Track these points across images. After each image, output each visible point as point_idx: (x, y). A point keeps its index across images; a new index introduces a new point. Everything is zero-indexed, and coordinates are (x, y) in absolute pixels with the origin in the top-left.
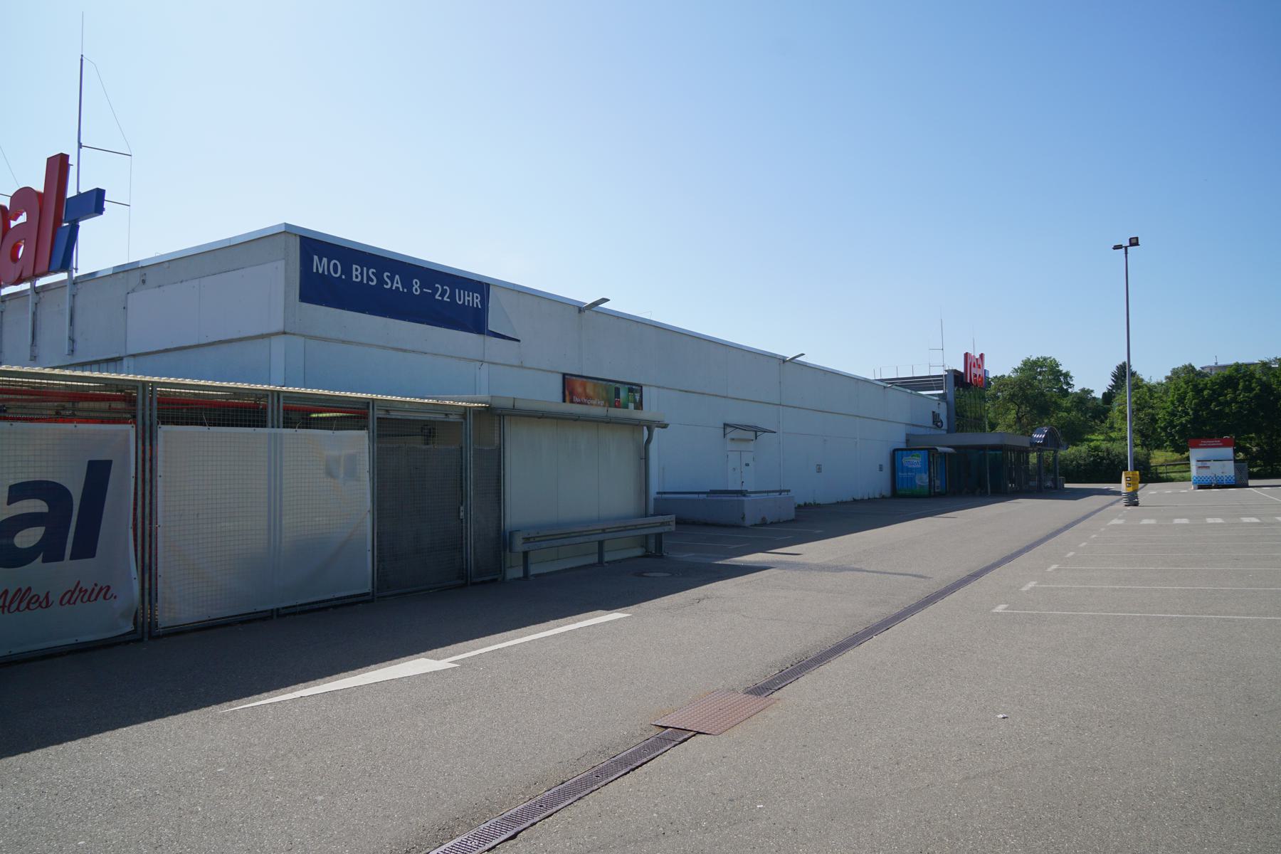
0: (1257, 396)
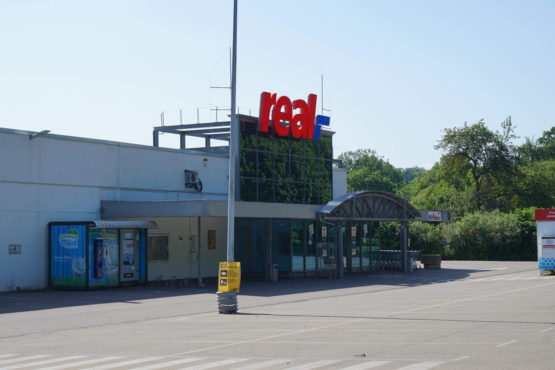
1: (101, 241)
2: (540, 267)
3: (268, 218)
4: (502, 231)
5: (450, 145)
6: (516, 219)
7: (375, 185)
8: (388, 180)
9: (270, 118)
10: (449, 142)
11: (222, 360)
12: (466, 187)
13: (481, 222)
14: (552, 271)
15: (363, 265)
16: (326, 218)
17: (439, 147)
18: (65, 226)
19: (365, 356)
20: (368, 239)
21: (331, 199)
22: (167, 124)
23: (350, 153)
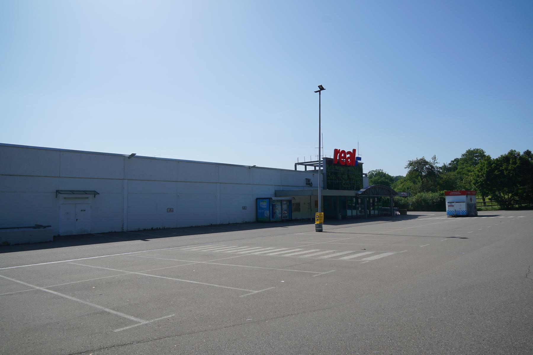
0: (518, 167)
1: (275, 205)
2: (447, 214)
3: (337, 196)
4: (432, 200)
5: (411, 167)
6: (438, 195)
7: (383, 183)
8: (388, 181)
9: (338, 159)
10: (410, 166)
11: (310, 250)
12: (418, 183)
13: (423, 196)
14: (452, 216)
15: (375, 213)
16: (360, 196)
17: (407, 168)
18: (262, 200)
19: (365, 249)
20: (377, 203)
21: (362, 188)
22: (299, 162)
23: (373, 171)
